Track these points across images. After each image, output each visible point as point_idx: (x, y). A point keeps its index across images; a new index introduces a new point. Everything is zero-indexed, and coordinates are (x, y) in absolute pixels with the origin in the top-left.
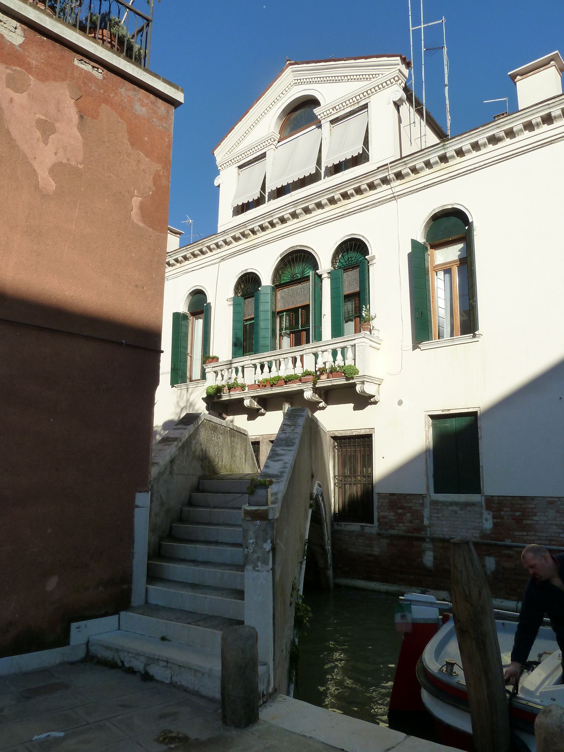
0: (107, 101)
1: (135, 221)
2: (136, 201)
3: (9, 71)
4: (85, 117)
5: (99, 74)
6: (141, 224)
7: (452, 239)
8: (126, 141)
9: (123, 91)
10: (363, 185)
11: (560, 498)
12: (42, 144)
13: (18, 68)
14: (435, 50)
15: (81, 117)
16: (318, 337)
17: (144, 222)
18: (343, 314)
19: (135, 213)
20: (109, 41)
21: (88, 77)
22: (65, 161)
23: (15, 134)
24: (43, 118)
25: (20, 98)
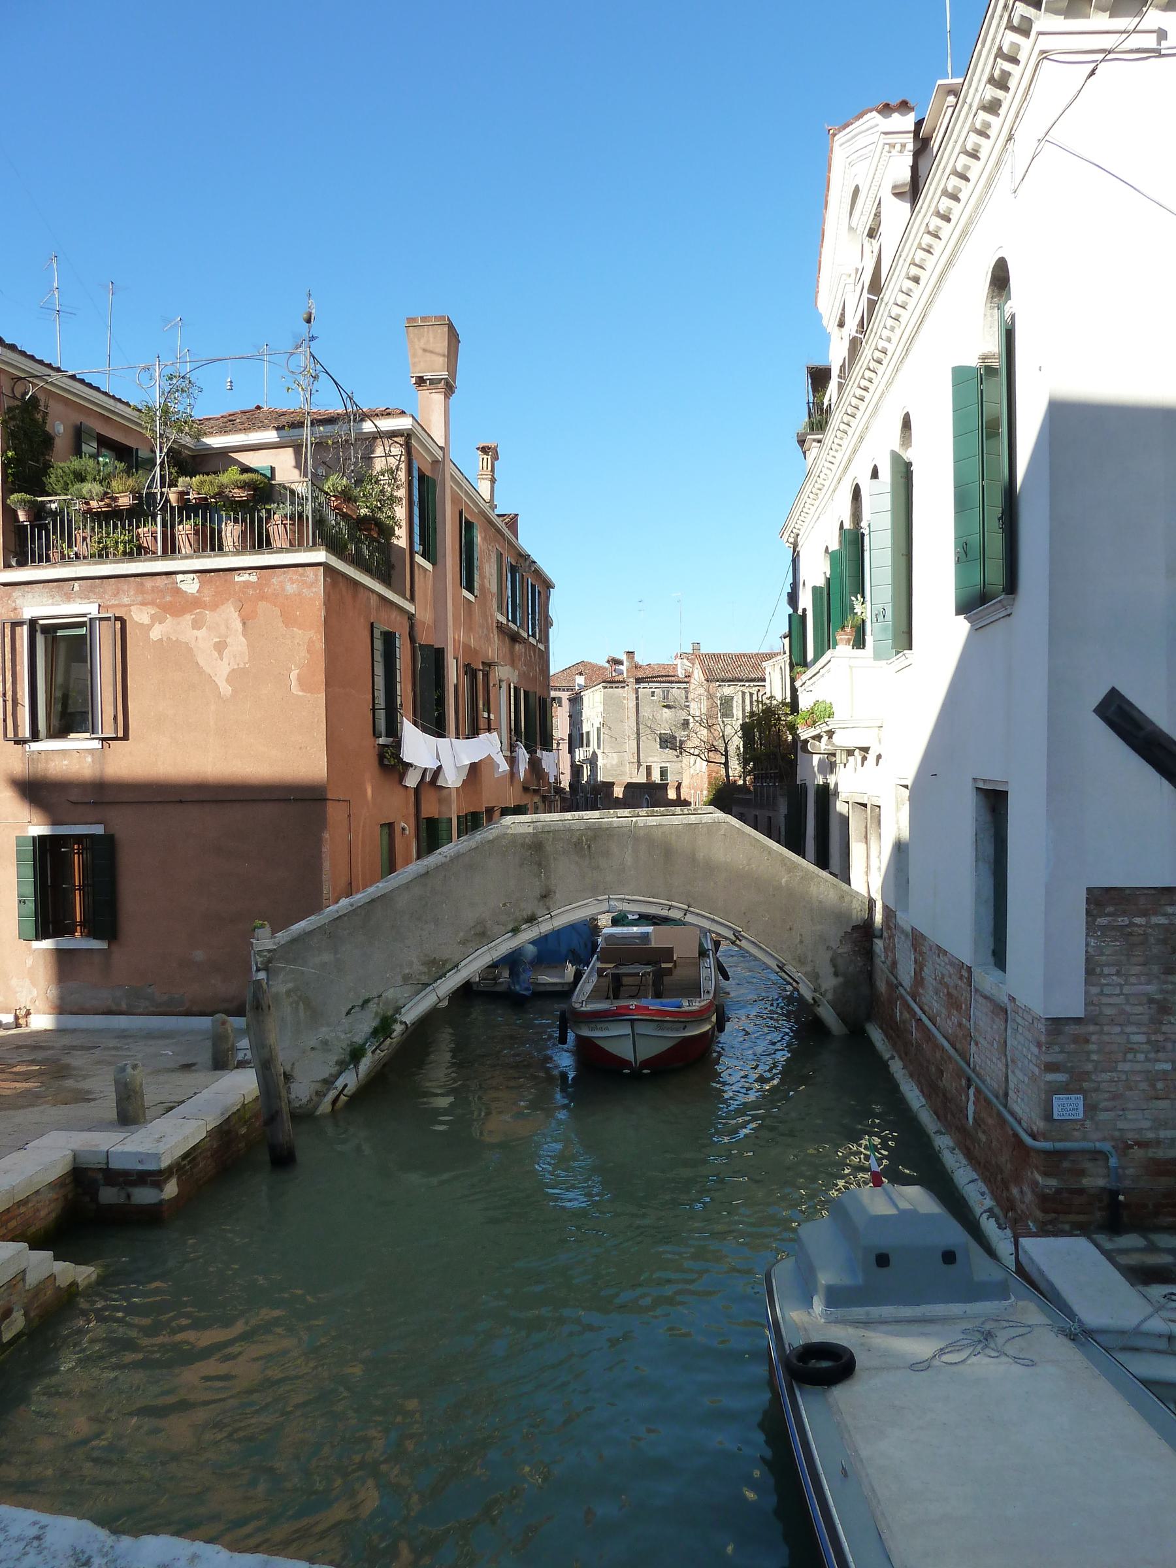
0: (263, 597)
1: (295, 693)
2: (294, 674)
3: (193, 617)
4: (247, 622)
5: (253, 578)
6: (301, 693)
7: (42, 1004)
8: (281, 625)
9: (274, 580)
10: (859, 136)
11: (180, 577)
12: (219, 661)
13: (198, 611)
14: (1125, 35)
15: (244, 624)
16: (458, 817)
17: (303, 690)
18: (799, 512)
19: (295, 688)
20: (238, 528)
21: (247, 584)
22: (236, 667)
23: (201, 663)
24: (218, 640)
25: (201, 633)
